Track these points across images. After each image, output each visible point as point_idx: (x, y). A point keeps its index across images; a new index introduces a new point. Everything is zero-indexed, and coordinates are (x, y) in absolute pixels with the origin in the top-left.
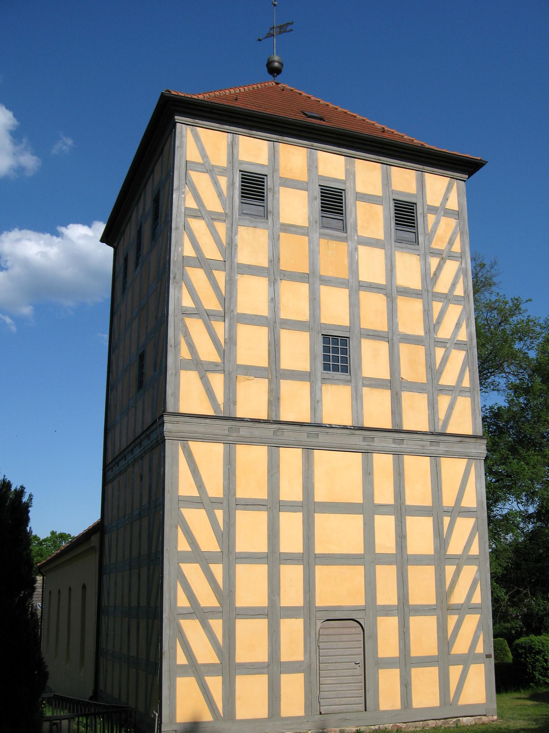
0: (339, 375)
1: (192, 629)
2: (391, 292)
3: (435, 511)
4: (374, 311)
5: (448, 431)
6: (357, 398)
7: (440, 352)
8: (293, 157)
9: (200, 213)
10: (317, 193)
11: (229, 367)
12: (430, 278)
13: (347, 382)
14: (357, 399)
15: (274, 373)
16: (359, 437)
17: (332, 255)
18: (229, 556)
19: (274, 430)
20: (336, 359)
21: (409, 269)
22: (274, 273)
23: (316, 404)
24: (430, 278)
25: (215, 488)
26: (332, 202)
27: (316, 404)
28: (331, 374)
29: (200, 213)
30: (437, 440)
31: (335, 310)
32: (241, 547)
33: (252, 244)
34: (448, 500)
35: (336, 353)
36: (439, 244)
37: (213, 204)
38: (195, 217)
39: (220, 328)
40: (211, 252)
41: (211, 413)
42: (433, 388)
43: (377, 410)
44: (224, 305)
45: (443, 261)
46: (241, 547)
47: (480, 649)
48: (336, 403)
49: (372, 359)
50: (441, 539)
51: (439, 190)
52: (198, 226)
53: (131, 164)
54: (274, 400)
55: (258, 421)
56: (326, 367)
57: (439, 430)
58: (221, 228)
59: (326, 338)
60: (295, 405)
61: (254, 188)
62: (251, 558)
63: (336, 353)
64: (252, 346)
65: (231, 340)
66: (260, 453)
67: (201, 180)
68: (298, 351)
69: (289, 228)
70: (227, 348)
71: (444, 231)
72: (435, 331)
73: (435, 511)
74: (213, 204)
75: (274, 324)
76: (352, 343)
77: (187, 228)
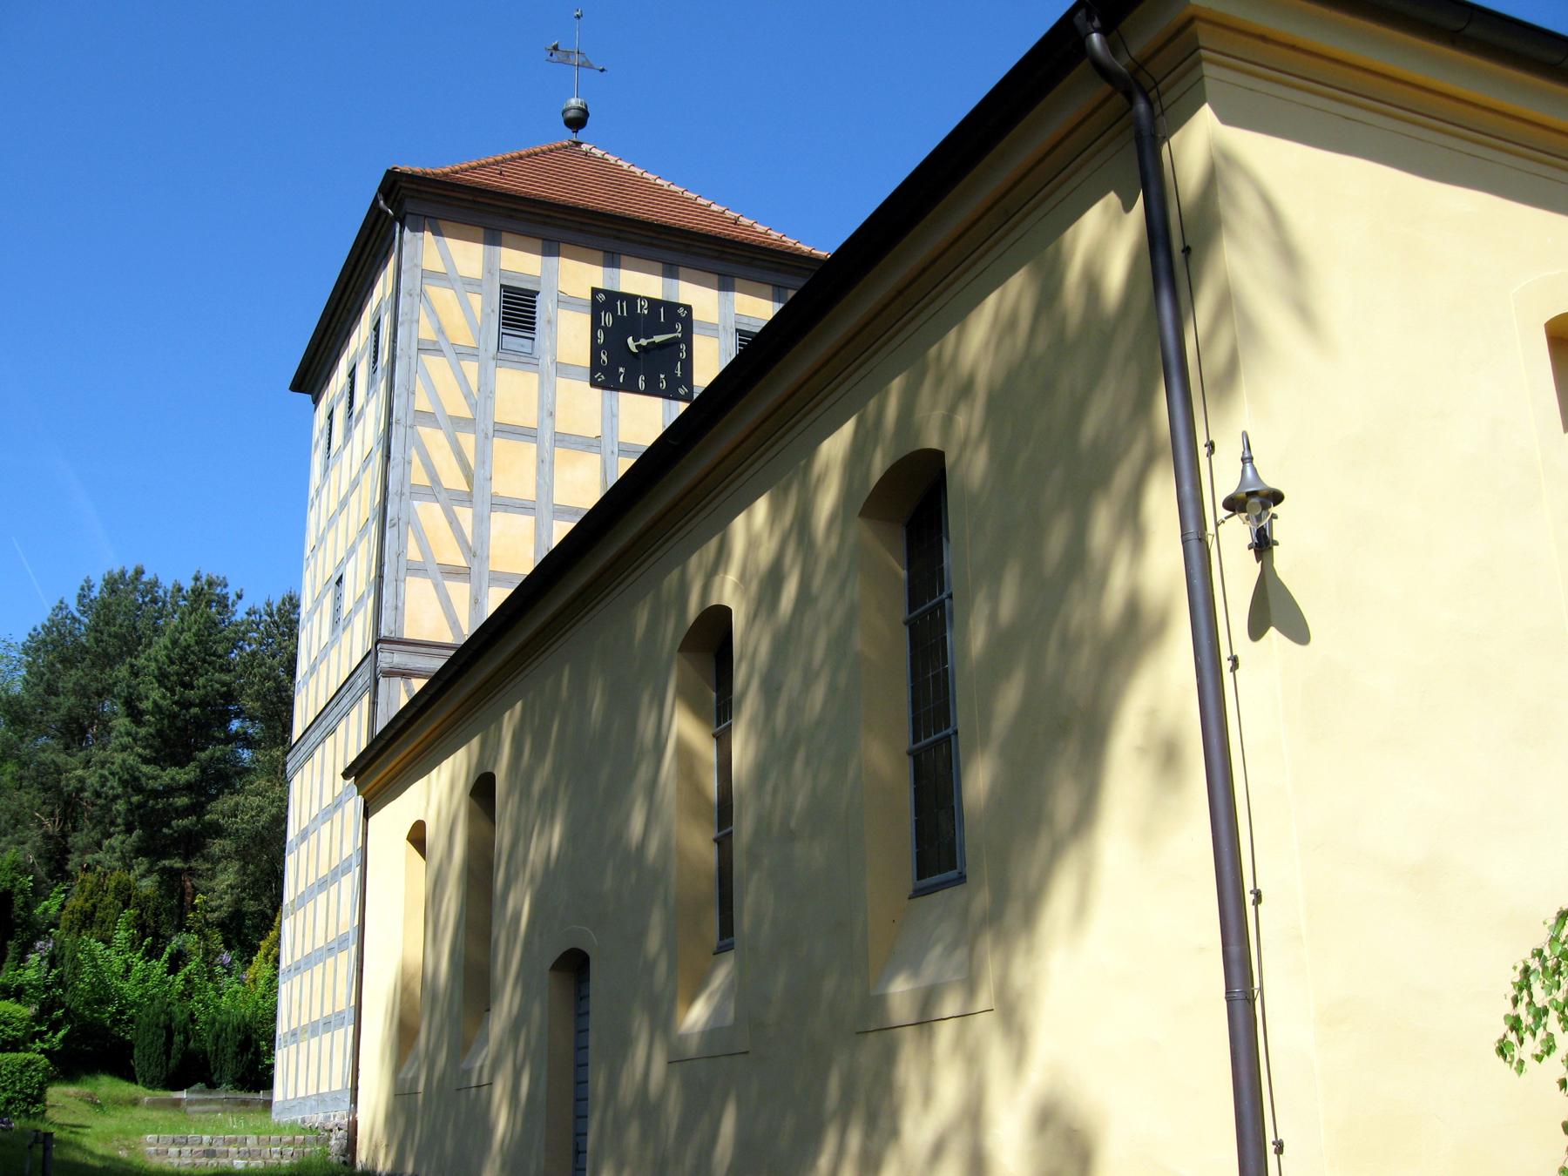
29: (429, 418)
37: (460, 332)
40: (453, 478)
58: (468, 441)
61: (518, 310)
69: (563, 369)
74: (460, 332)
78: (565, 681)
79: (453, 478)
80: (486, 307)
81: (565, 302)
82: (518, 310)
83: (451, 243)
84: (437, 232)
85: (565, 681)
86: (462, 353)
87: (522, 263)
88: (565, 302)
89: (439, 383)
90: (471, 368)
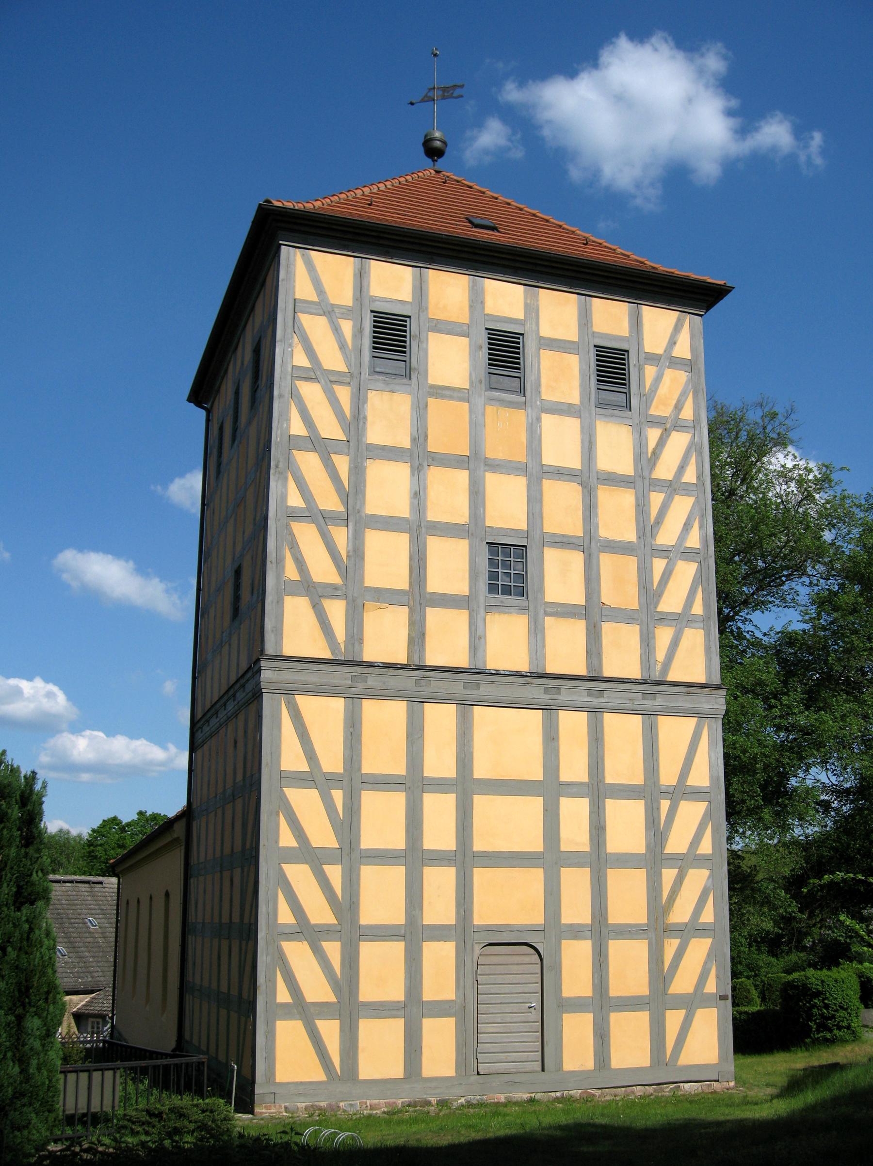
1: (297, 953)
2: (589, 480)
3: (649, 792)
4: (562, 508)
5: (670, 678)
6: (537, 633)
8: (557, 313)
11: (355, 593)
12: (647, 460)
13: (523, 609)
14: (537, 633)
15: (417, 598)
16: (539, 688)
17: (504, 430)
18: (351, 853)
19: (416, 679)
21: (615, 447)
22: (419, 457)
25: (332, 760)
26: (505, 352)
30: (652, 691)
31: (507, 506)
32: (368, 841)
34: (668, 776)
35: (507, 569)
36: (661, 408)
37: (333, 360)
39: (341, 536)
40: (320, 912)
41: (327, 654)
42: (647, 616)
43: (565, 650)
44: (346, 503)
46: (368, 841)
48: (507, 642)
49: (560, 577)
50: (657, 832)
51: (661, 328)
54: (417, 637)
56: (493, 588)
57: (656, 675)
58: (344, 394)
60: (447, 645)
63: (507, 569)
64: (386, 560)
65: (357, 552)
66: (398, 709)
68: (451, 567)
69: (442, 392)
72: (653, 536)
73: (649, 792)
74: (333, 360)
75: (419, 529)
76: (531, 554)
77: (295, 394)
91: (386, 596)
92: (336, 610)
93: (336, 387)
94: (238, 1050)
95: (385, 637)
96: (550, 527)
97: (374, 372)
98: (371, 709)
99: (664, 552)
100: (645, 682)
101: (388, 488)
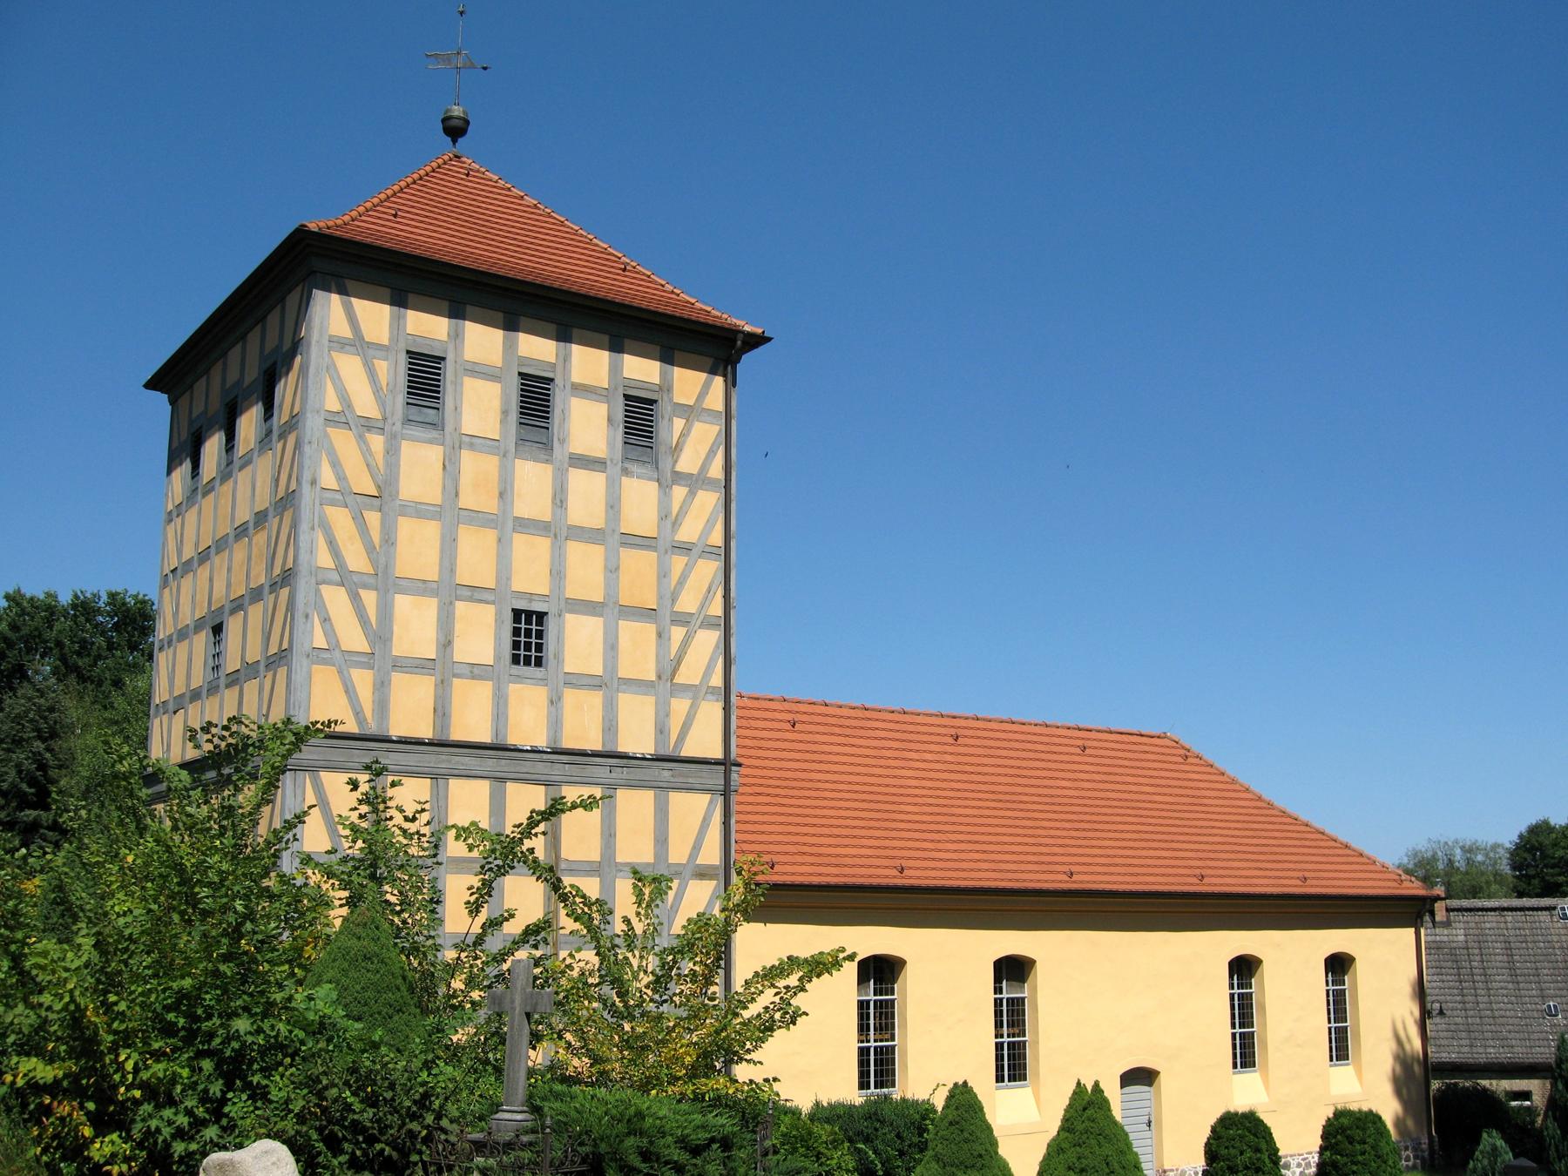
0: (531, 671)
4: (586, 571)
7: (678, 633)
9: (342, 419)
10: (515, 383)
11: (381, 658)
12: (670, 518)
13: (543, 681)
14: (555, 701)
15: (442, 668)
17: (533, 481)
18: (385, 580)
19: (443, 752)
20: (528, 646)
21: (641, 499)
22: (450, 514)
23: (500, 714)
24: (670, 518)
26: (535, 400)
27: (500, 714)
28: (522, 670)
29: (342, 419)
31: (530, 578)
32: (400, 648)
33: (420, 467)
35: (529, 637)
36: (688, 462)
37: (365, 404)
38: (333, 503)
39: (373, 518)
40: (357, 560)
43: (584, 732)
45: (692, 494)
46: (400, 648)
47: (679, 424)
48: (528, 729)
49: (577, 642)
51: (690, 384)
52: (343, 441)
53: (256, 266)
55: (419, 742)
56: (516, 660)
57: (669, 751)
58: (377, 442)
59: (517, 614)
60: (472, 723)
61: (425, 378)
62: (419, 511)
63: (529, 637)
64: (415, 626)
65: (389, 540)
67: (350, 367)
68: (481, 636)
69: (474, 443)
70: (382, 550)
71: (695, 444)
72: (674, 601)
74: (365, 404)
76: (551, 626)
77: (332, 369)
78: (519, 1117)
79: (357, 560)
80: (392, 371)
81: (478, 371)
82: (425, 378)
83: (359, 305)
84: (343, 291)
85: (519, 1117)
86: (368, 425)
87: (428, 327)
88: (478, 371)
89: (338, 460)
90: (377, 442)
91: (419, 511)
92: (363, 680)
93: (362, 592)
94: (293, 618)
95: (410, 715)
96: (573, 591)
97: (408, 421)
98: (677, 799)
99: (685, 548)
100: (658, 759)
101: (417, 547)
